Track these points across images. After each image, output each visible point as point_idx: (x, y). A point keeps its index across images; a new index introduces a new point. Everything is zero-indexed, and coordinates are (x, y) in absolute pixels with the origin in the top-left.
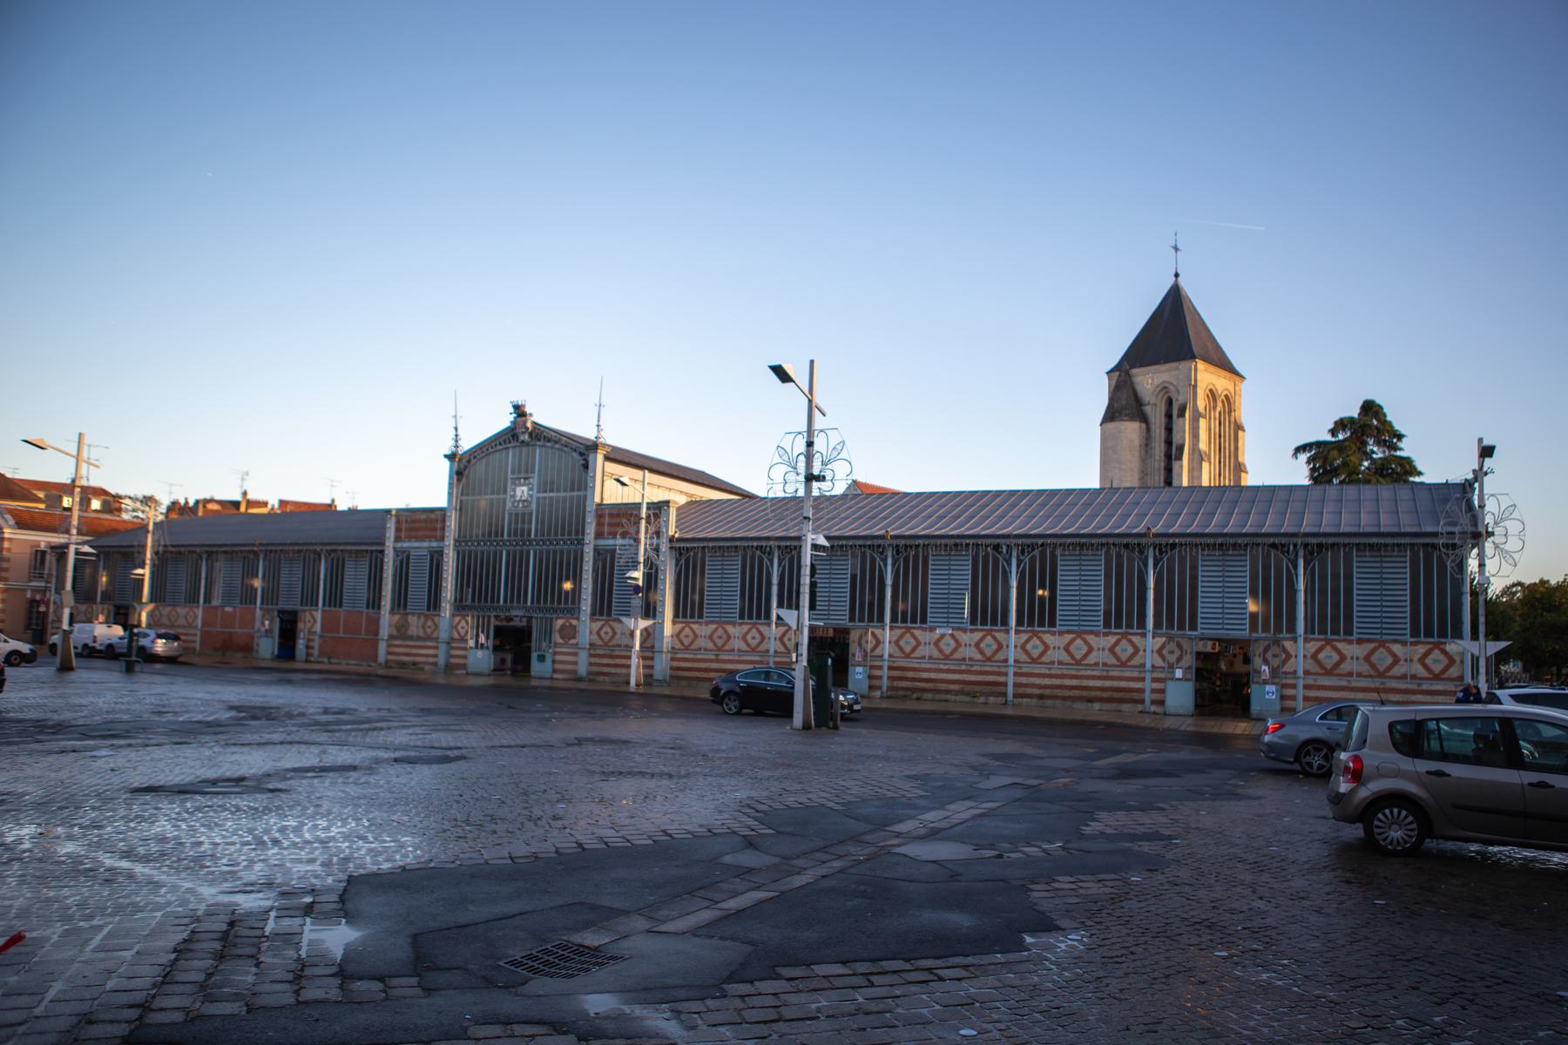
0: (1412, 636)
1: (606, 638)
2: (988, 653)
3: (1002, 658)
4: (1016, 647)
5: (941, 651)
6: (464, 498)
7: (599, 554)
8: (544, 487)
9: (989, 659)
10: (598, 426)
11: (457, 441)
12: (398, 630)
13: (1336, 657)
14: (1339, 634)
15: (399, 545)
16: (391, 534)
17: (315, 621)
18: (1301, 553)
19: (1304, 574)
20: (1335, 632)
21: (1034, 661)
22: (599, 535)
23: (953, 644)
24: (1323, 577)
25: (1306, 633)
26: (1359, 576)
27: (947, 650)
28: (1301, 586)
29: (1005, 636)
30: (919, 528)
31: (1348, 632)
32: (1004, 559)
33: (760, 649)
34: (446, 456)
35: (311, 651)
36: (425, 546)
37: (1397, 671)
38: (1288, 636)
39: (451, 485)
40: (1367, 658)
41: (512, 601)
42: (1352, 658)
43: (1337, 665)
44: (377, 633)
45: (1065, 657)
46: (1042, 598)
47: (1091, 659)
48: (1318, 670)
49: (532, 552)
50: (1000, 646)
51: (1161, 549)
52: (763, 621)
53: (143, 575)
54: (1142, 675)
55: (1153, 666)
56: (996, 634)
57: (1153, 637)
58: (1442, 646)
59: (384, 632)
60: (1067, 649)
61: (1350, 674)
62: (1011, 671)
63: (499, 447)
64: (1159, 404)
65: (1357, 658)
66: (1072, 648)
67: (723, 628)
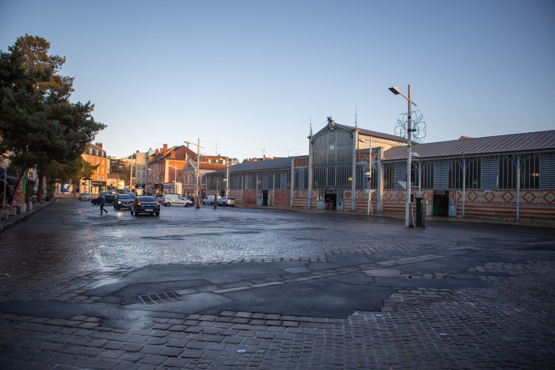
0: (500, 188)
2: (507, 200)
4: (520, 197)
5: (486, 199)
6: (314, 151)
7: (358, 167)
10: (356, 122)
11: (311, 132)
15: (295, 168)
16: (293, 164)
21: (529, 203)
34: (308, 137)
36: (301, 168)
41: (330, 185)
42: (482, 196)
50: (513, 197)
60: (544, 198)
62: (518, 207)
63: (324, 133)
65: (497, 197)
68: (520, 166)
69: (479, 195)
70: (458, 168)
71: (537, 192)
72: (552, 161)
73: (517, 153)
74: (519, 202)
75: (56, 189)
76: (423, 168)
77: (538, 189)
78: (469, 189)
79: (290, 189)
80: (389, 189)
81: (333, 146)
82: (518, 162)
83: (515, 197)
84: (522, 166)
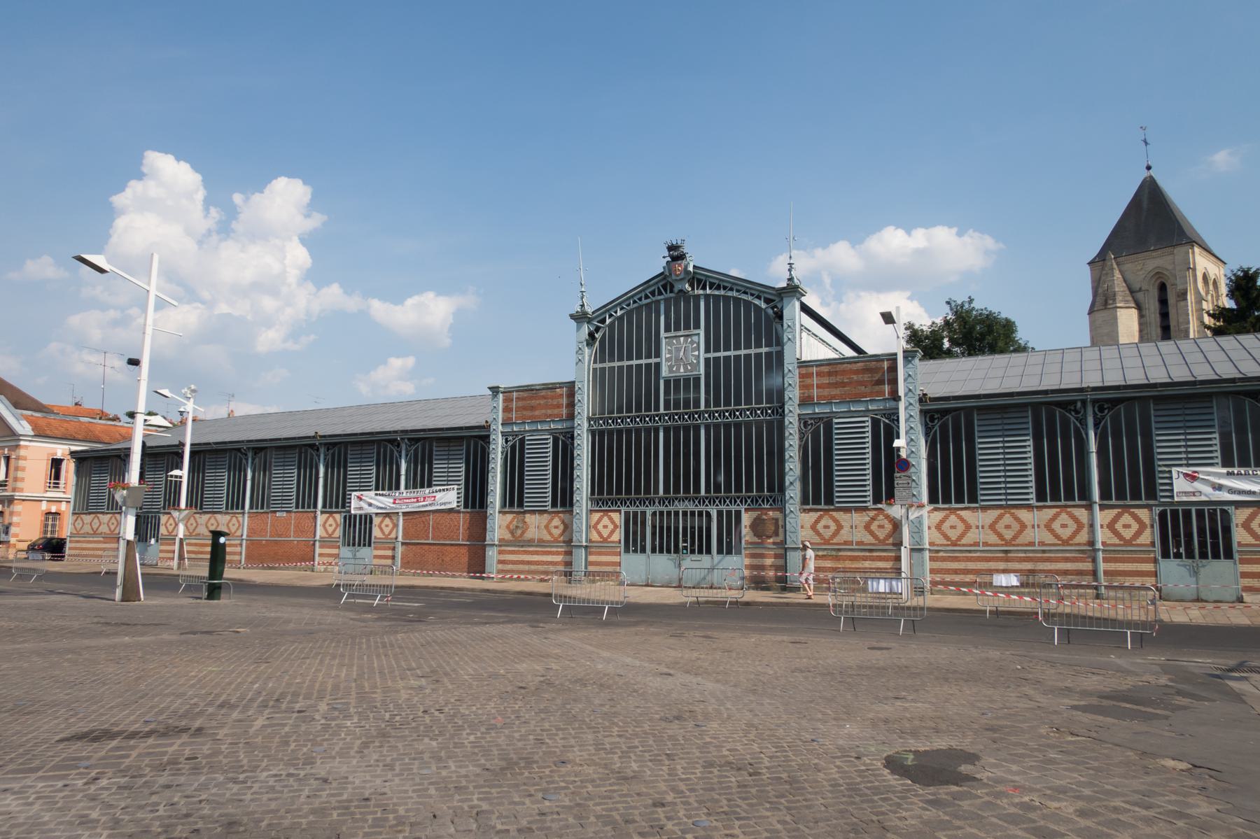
0: (1038, 500)
4: (929, 528)
7: (806, 424)
12: (512, 533)
17: (324, 526)
34: (572, 316)
41: (677, 490)
42: (1038, 526)
52: (239, 511)
53: (181, 477)
65: (983, 527)
69: (1029, 524)
72: (287, 460)
74: (1100, 541)
75: (699, 599)
76: (1105, 427)
79: (572, 505)
83: (974, 527)
84: (1100, 434)
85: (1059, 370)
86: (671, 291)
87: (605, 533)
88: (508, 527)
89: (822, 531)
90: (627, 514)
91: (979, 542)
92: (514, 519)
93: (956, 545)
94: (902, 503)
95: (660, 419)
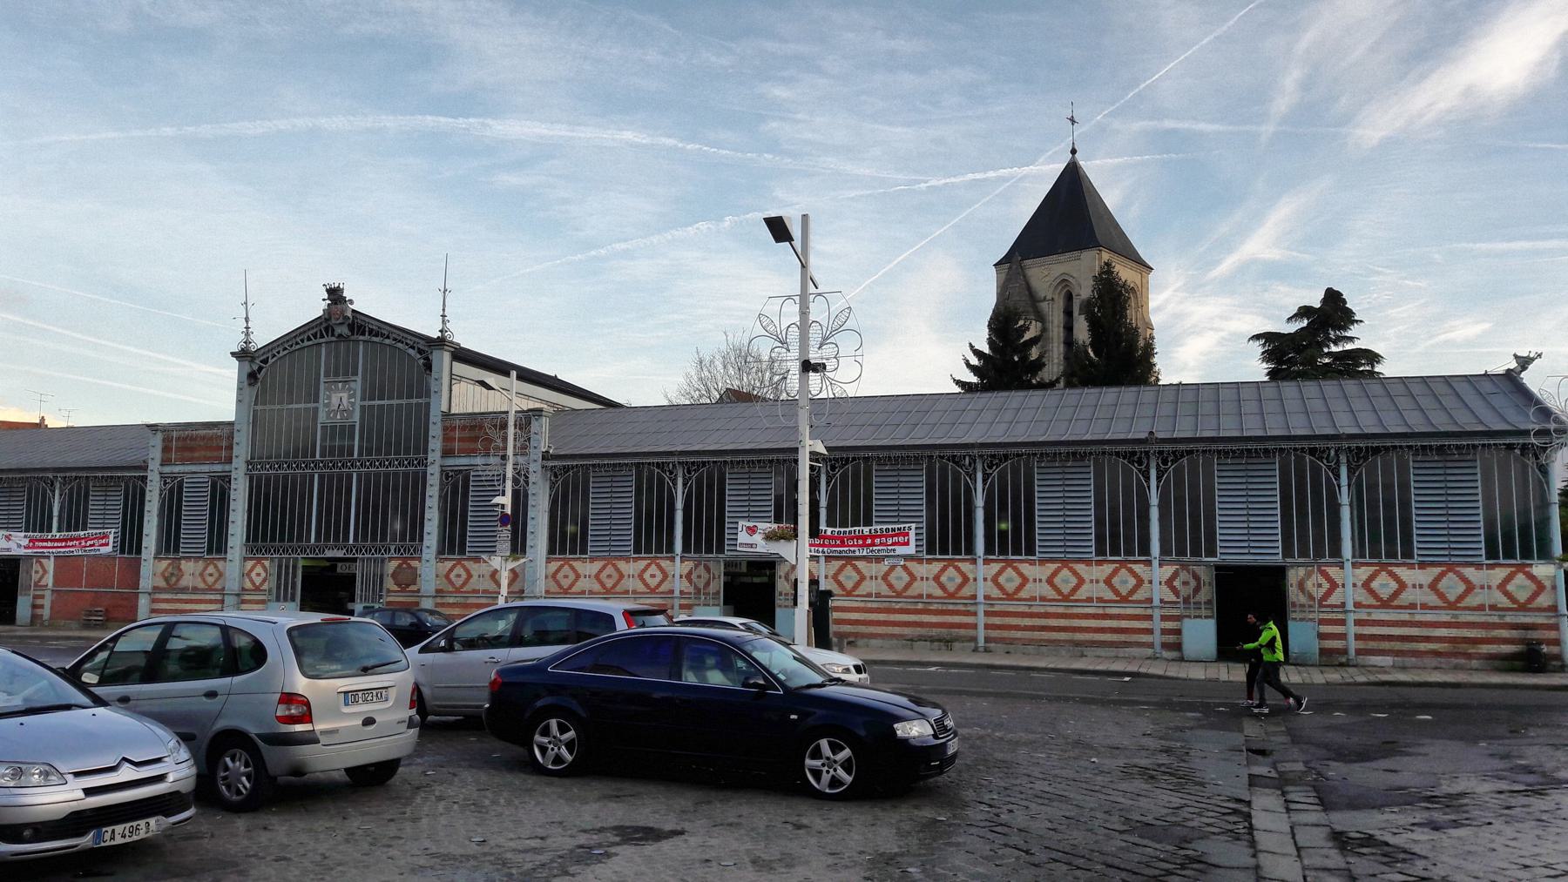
1: (458, 582)
2: (951, 588)
3: (220, 587)
5: (890, 586)
6: (259, 407)
7: (447, 477)
8: (370, 392)
9: (952, 596)
10: (443, 316)
11: (247, 334)
12: (167, 580)
13: (1394, 585)
14: (1396, 557)
15: (167, 469)
16: (156, 454)
17: (45, 572)
18: (1343, 459)
19: (1349, 485)
20: (1391, 554)
21: (1010, 597)
22: (447, 453)
23: (907, 578)
24: (1372, 487)
25: (1354, 557)
26: (1417, 485)
27: (899, 585)
28: (1154, 500)
29: (972, 567)
30: (73, 459)
31: (1408, 554)
32: (967, 474)
33: (662, 589)
34: (233, 354)
35: (39, 611)
36: (201, 471)
37: (1472, 601)
38: (1332, 560)
39: (240, 389)
40: (1433, 586)
42: (589, 577)
43: (1396, 594)
44: (136, 585)
45: (1049, 592)
46: (1002, 518)
47: (1083, 593)
48: (1372, 601)
49: (316, 476)
50: (966, 579)
51: (689, 468)
54: (1149, 612)
55: (1162, 601)
56: (1134, 567)
57: (1161, 565)
58: (1527, 569)
59: (146, 582)
60: (1050, 581)
61: (1412, 606)
62: (981, 609)
63: (307, 343)
64: (1056, 297)
66: (1057, 580)
67: (614, 565)
68: (683, 493)
69: (867, 575)
70: (660, 491)
71: (1031, 564)
73: (976, 451)
77: (587, 556)
78: (643, 555)
80: (568, 556)
81: (345, 395)
82: (979, 476)
85: (1150, 413)
86: (333, 335)
87: (258, 581)
88: (163, 574)
89: (1117, 586)
90: (280, 560)
91: (1036, 597)
92: (169, 565)
93: (566, 594)
94: (501, 554)
95: (334, 466)
